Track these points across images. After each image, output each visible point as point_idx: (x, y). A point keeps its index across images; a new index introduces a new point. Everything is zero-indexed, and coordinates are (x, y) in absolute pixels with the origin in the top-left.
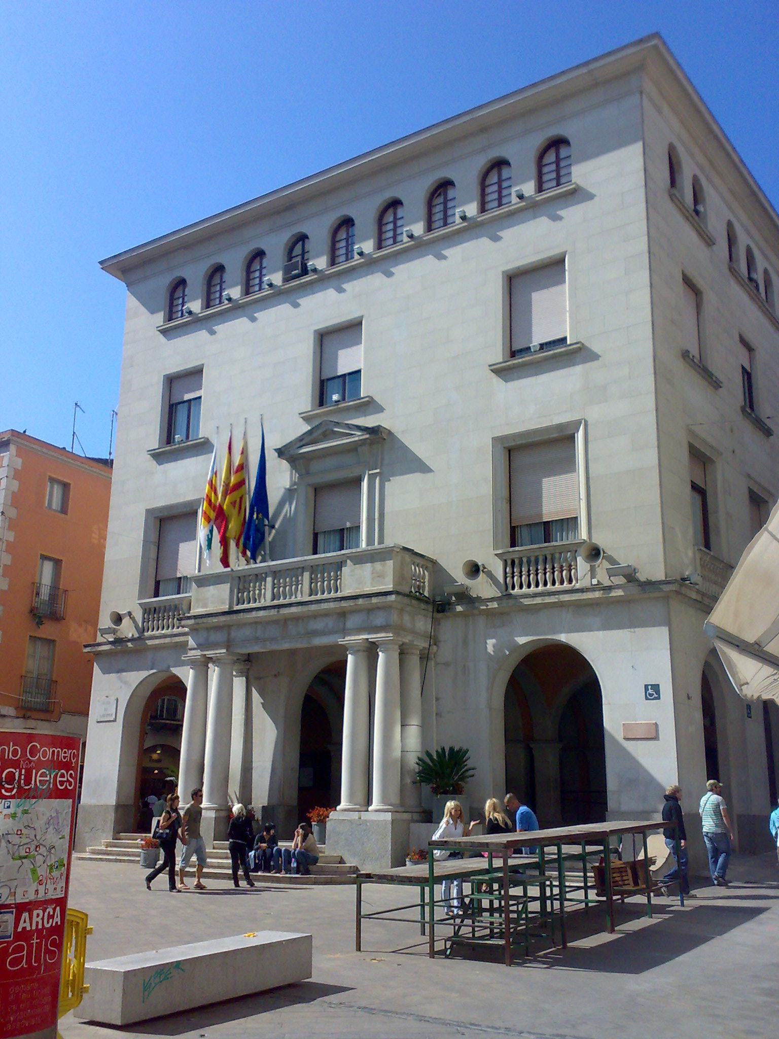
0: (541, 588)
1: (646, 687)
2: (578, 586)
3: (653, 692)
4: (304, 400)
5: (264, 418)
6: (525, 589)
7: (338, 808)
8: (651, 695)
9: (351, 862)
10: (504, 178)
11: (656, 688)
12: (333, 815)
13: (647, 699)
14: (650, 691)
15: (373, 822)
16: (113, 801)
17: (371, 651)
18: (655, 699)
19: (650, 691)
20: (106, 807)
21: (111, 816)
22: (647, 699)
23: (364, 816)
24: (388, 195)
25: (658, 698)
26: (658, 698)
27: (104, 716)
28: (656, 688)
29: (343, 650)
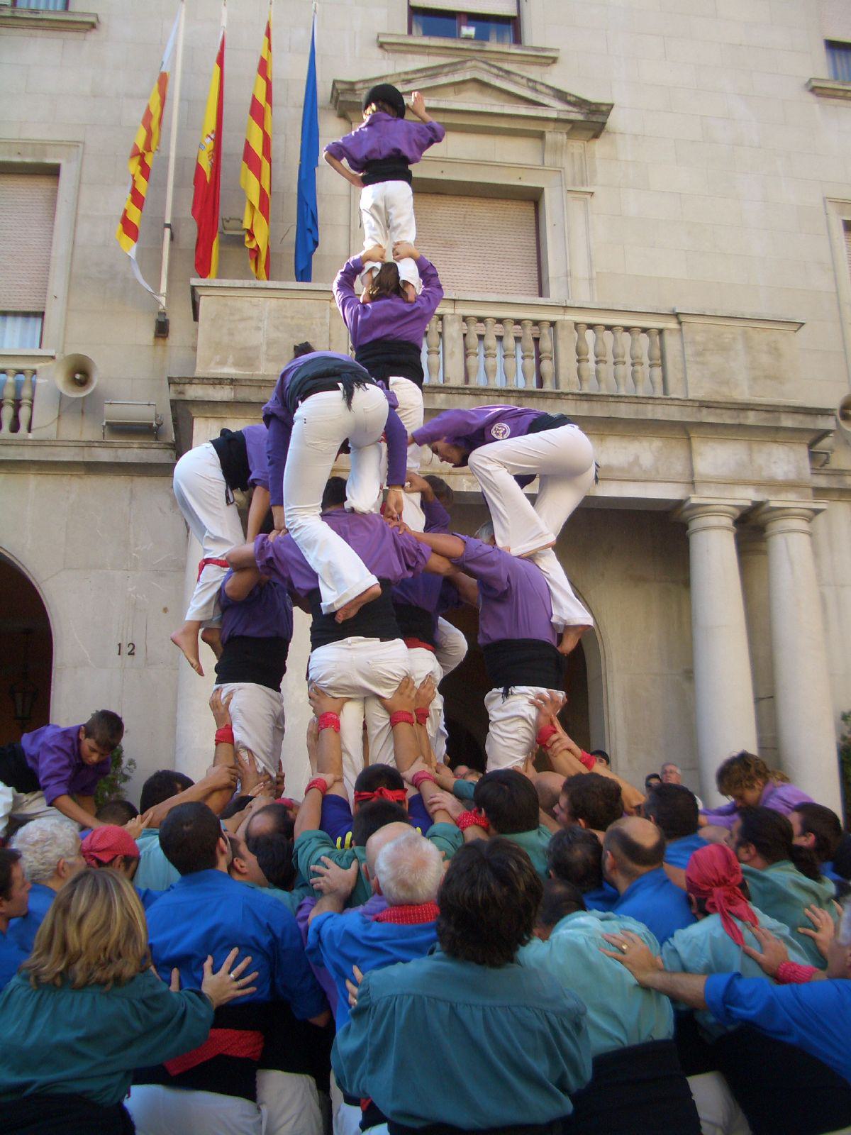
2: (30, 436)
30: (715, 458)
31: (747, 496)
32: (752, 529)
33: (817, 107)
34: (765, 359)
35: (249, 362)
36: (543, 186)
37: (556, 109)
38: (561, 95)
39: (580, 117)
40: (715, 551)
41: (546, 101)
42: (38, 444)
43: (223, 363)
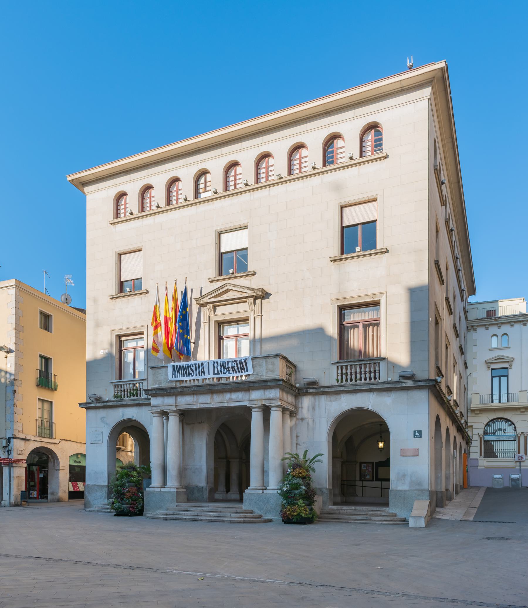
0: (358, 382)
1: (415, 431)
3: (418, 434)
4: (212, 271)
5: (178, 282)
6: (358, 382)
7: (249, 488)
8: (417, 436)
9: (257, 512)
10: (238, 173)
11: (420, 432)
12: (246, 491)
13: (414, 437)
14: (417, 434)
15: (270, 494)
16: (106, 483)
17: (266, 411)
18: (419, 437)
19: (417, 434)
20: (103, 486)
21: (105, 490)
22: (414, 437)
23: (163, 490)
24: (333, 129)
25: (421, 437)
26: (421, 437)
27: (95, 441)
28: (420, 432)
29: (248, 410)
30: (256, 395)
31: (259, 404)
32: (266, 411)
33: (333, 266)
34: (270, 366)
35: (160, 383)
36: (379, 299)
37: (249, 293)
38: (249, 288)
39: (254, 294)
40: (256, 418)
41: (245, 291)
42: (382, 383)
43: (156, 384)
